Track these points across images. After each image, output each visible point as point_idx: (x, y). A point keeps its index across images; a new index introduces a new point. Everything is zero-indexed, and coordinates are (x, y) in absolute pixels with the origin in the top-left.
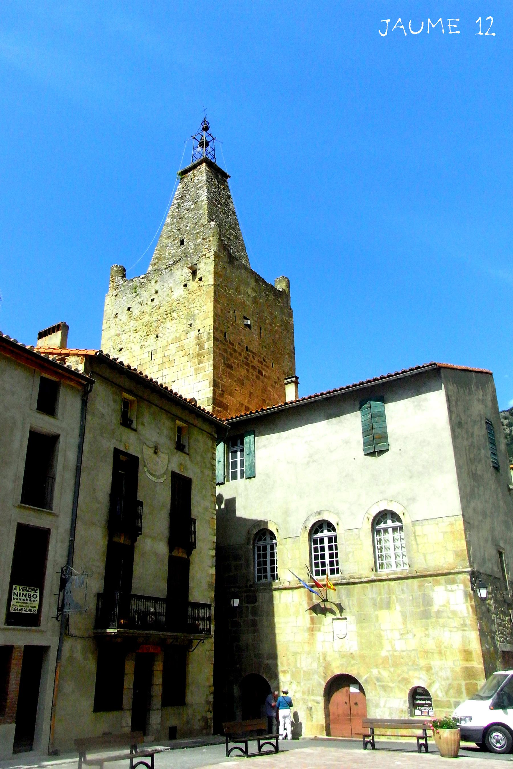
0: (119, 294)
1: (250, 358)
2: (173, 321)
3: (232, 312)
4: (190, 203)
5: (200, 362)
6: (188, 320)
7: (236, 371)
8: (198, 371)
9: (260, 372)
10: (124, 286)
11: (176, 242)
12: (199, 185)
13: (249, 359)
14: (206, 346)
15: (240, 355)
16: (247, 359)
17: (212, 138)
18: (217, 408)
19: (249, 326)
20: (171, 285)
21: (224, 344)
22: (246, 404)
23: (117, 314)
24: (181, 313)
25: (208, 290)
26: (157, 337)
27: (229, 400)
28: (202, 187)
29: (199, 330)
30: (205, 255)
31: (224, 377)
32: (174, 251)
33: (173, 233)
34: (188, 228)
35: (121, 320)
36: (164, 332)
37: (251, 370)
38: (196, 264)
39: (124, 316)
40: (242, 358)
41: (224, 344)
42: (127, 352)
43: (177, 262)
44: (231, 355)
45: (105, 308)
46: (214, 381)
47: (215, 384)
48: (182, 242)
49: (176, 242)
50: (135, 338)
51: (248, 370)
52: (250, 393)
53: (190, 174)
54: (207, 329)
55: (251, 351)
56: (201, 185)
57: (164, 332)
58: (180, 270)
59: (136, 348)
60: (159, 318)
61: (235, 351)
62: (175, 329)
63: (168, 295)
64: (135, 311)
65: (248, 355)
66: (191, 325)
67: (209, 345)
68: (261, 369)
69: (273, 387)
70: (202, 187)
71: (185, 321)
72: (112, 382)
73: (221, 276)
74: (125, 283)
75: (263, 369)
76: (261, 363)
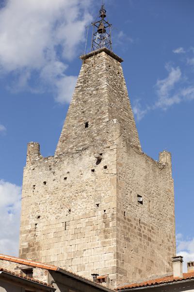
0: (36, 169)
1: (143, 229)
2: (83, 200)
3: (129, 194)
4: (93, 89)
5: (106, 237)
6: (95, 201)
7: (133, 241)
8: (104, 244)
9: (150, 239)
10: (40, 162)
11: (81, 123)
12: (100, 73)
13: (142, 230)
14: (111, 225)
15: (135, 228)
16: (140, 230)
17: (108, 25)
18: (119, 275)
19: (141, 203)
20: (81, 168)
21: (124, 222)
22: (139, 268)
23: (34, 186)
24: (89, 194)
25: (112, 178)
26: (70, 211)
27: (129, 267)
28: (102, 75)
29: (105, 211)
30: (109, 147)
31: (124, 249)
32: (79, 132)
33: (78, 114)
34: (91, 112)
35: (38, 192)
36: (75, 207)
37: (143, 239)
38: (101, 154)
39: (40, 188)
40: (136, 231)
41: (124, 222)
42: (44, 220)
43: (85, 149)
44: (129, 229)
45: (24, 179)
46: (117, 253)
47: (118, 256)
48: (87, 125)
49: (81, 123)
50: (51, 209)
51: (141, 240)
52: (143, 257)
53: (90, 59)
54: (112, 210)
55: (144, 224)
56: (101, 73)
57: (75, 207)
58: (88, 156)
59: (52, 218)
60: (71, 195)
61: (132, 225)
62: (85, 207)
63: (78, 177)
64: (51, 185)
65: (141, 227)
66: (98, 205)
67: (113, 224)
68: (150, 237)
69: (159, 249)
70: (102, 75)
71: (93, 201)
72: (64, 285)
73: (121, 165)
74: (41, 160)
75: (152, 236)
76: (150, 231)
